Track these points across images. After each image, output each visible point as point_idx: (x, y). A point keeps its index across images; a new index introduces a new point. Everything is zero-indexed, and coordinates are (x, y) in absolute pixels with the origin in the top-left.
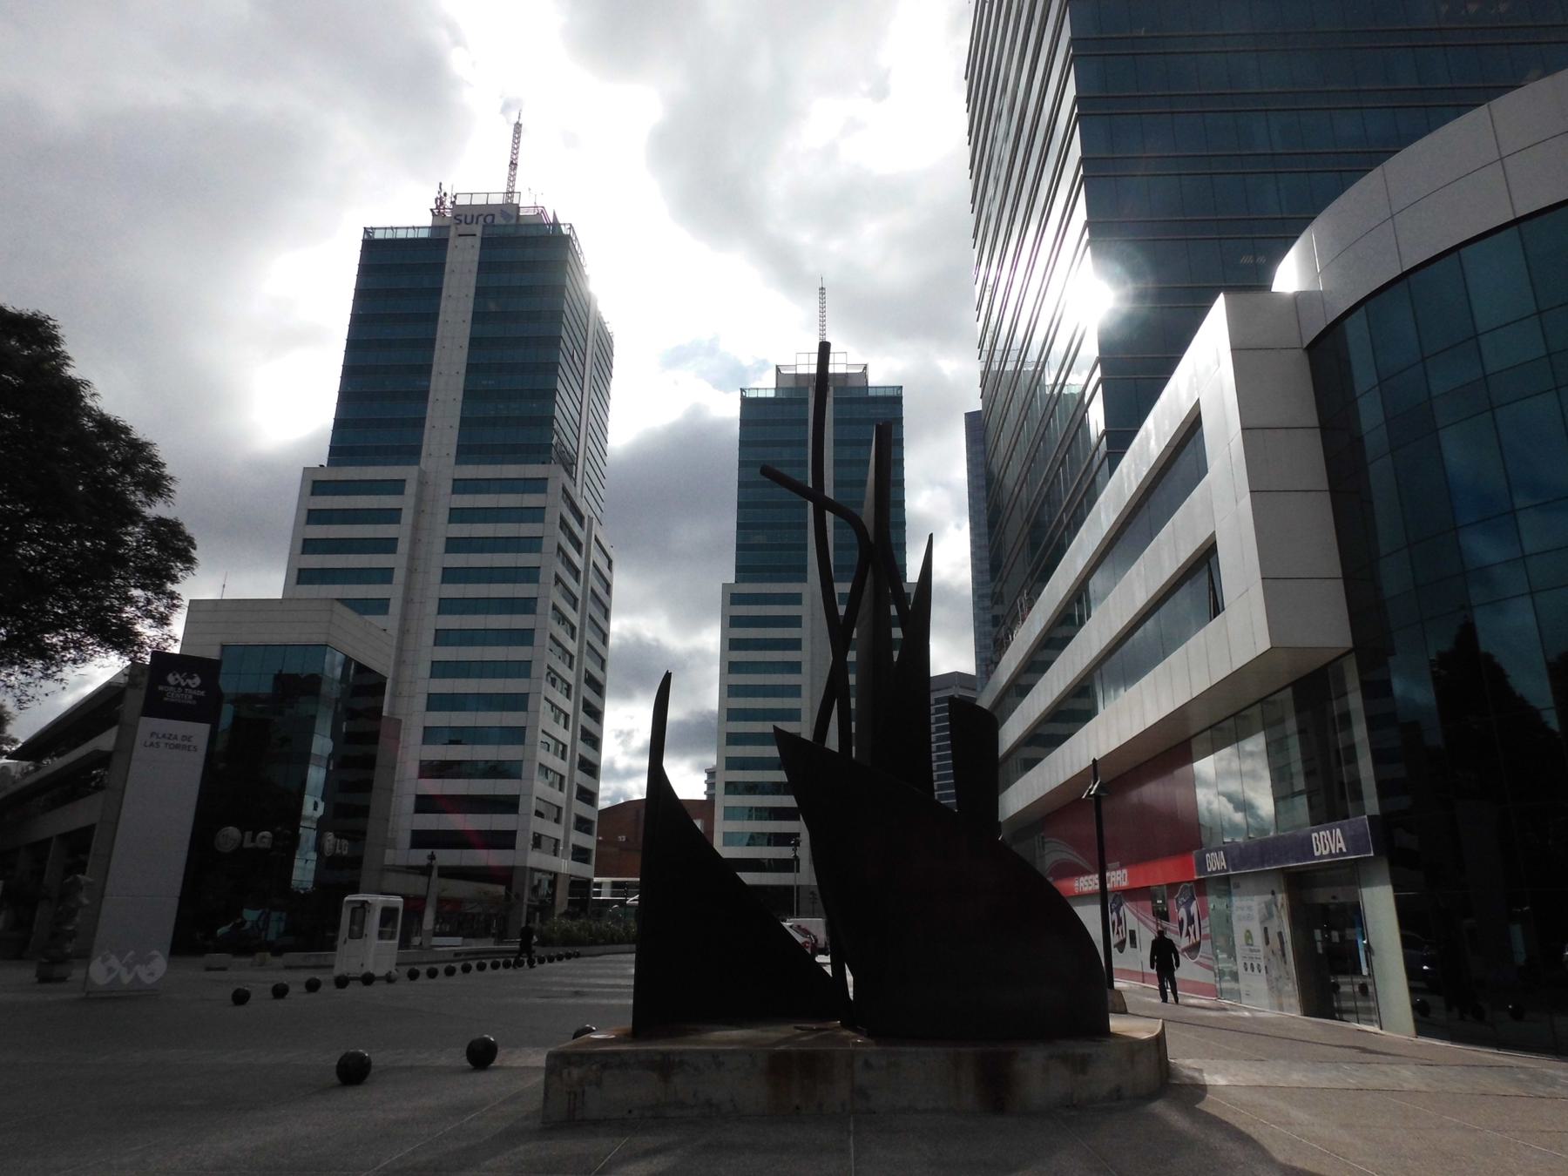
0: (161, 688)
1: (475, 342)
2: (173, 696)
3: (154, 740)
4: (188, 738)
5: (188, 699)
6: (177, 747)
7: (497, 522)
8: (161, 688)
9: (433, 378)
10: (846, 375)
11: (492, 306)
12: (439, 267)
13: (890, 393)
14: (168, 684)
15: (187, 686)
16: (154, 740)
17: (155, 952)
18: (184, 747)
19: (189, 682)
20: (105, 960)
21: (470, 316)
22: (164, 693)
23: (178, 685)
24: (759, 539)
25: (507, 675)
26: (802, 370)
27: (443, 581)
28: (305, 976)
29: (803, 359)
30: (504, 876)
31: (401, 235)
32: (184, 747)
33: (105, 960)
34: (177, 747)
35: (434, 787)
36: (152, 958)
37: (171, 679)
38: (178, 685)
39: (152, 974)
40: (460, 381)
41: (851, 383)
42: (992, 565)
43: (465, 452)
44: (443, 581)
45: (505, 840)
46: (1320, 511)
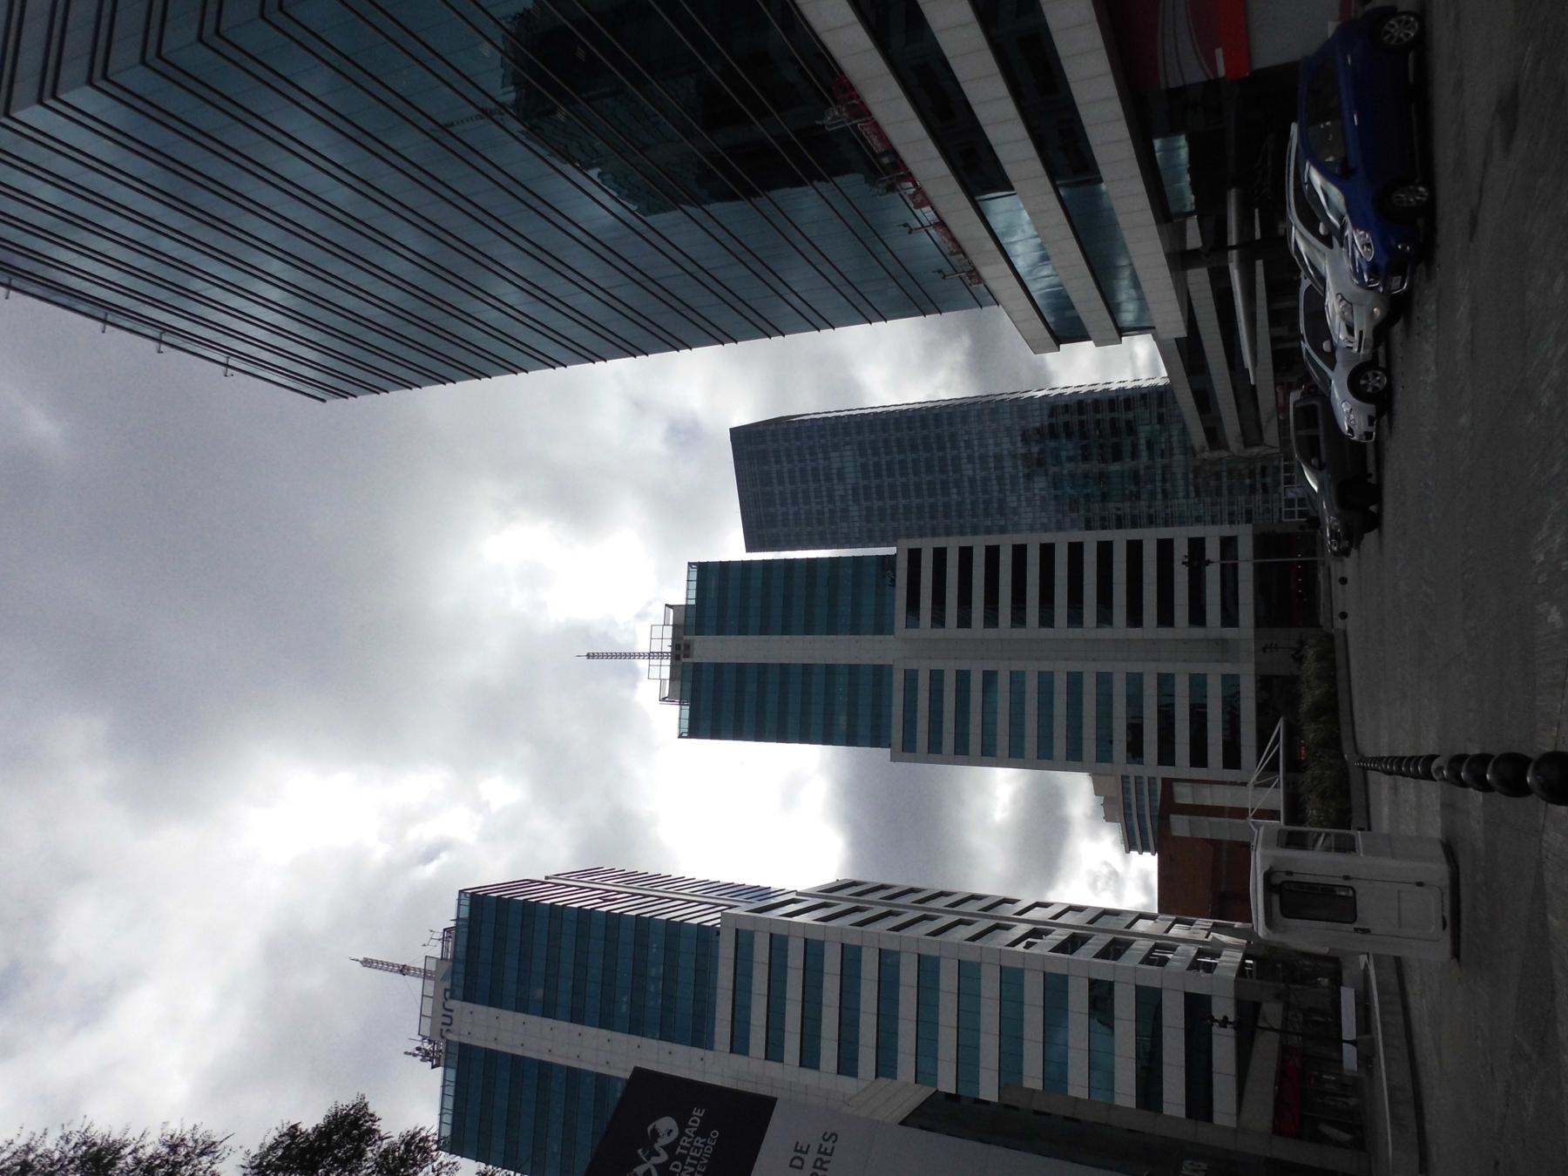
1: (577, 1017)
7: (896, 1051)
9: (614, 1073)
10: (675, 626)
11: (539, 993)
12: (491, 1056)
13: (694, 576)
21: (604, 1032)
24: (842, 721)
25: (1019, 1039)
26: (666, 673)
27: (817, 1067)
29: (655, 673)
30: (1247, 1023)
31: (449, 1104)
35: (1003, 682)
40: (590, 1031)
41: (682, 621)
43: (700, 1037)
44: (817, 1067)
45: (1197, 1006)
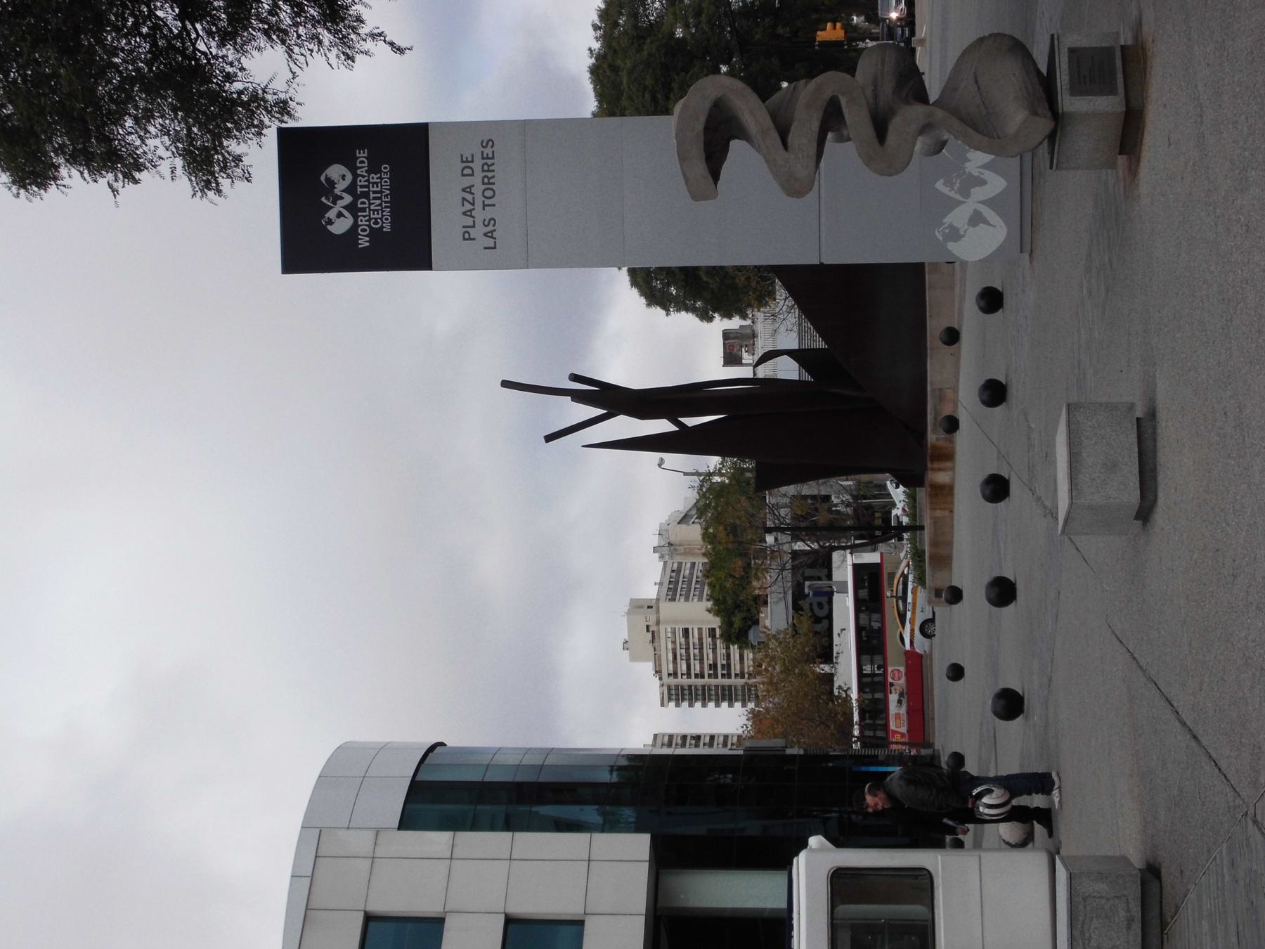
0: (364, 242)
2: (379, 214)
3: (478, 232)
4: (467, 161)
5: (381, 182)
6: (488, 182)
8: (364, 242)
14: (353, 231)
15: (351, 190)
16: (478, 232)
17: (323, 178)
18: (487, 168)
19: (341, 186)
20: (955, 235)
22: (375, 234)
23: (352, 208)
28: (970, 318)
32: (487, 168)
33: (955, 235)
34: (488, 182)
36: (328, 179)
37: (340, 226)
38: (352, 208)
39: (343, 177)
42: (722, 607)
46: (474, 776)
